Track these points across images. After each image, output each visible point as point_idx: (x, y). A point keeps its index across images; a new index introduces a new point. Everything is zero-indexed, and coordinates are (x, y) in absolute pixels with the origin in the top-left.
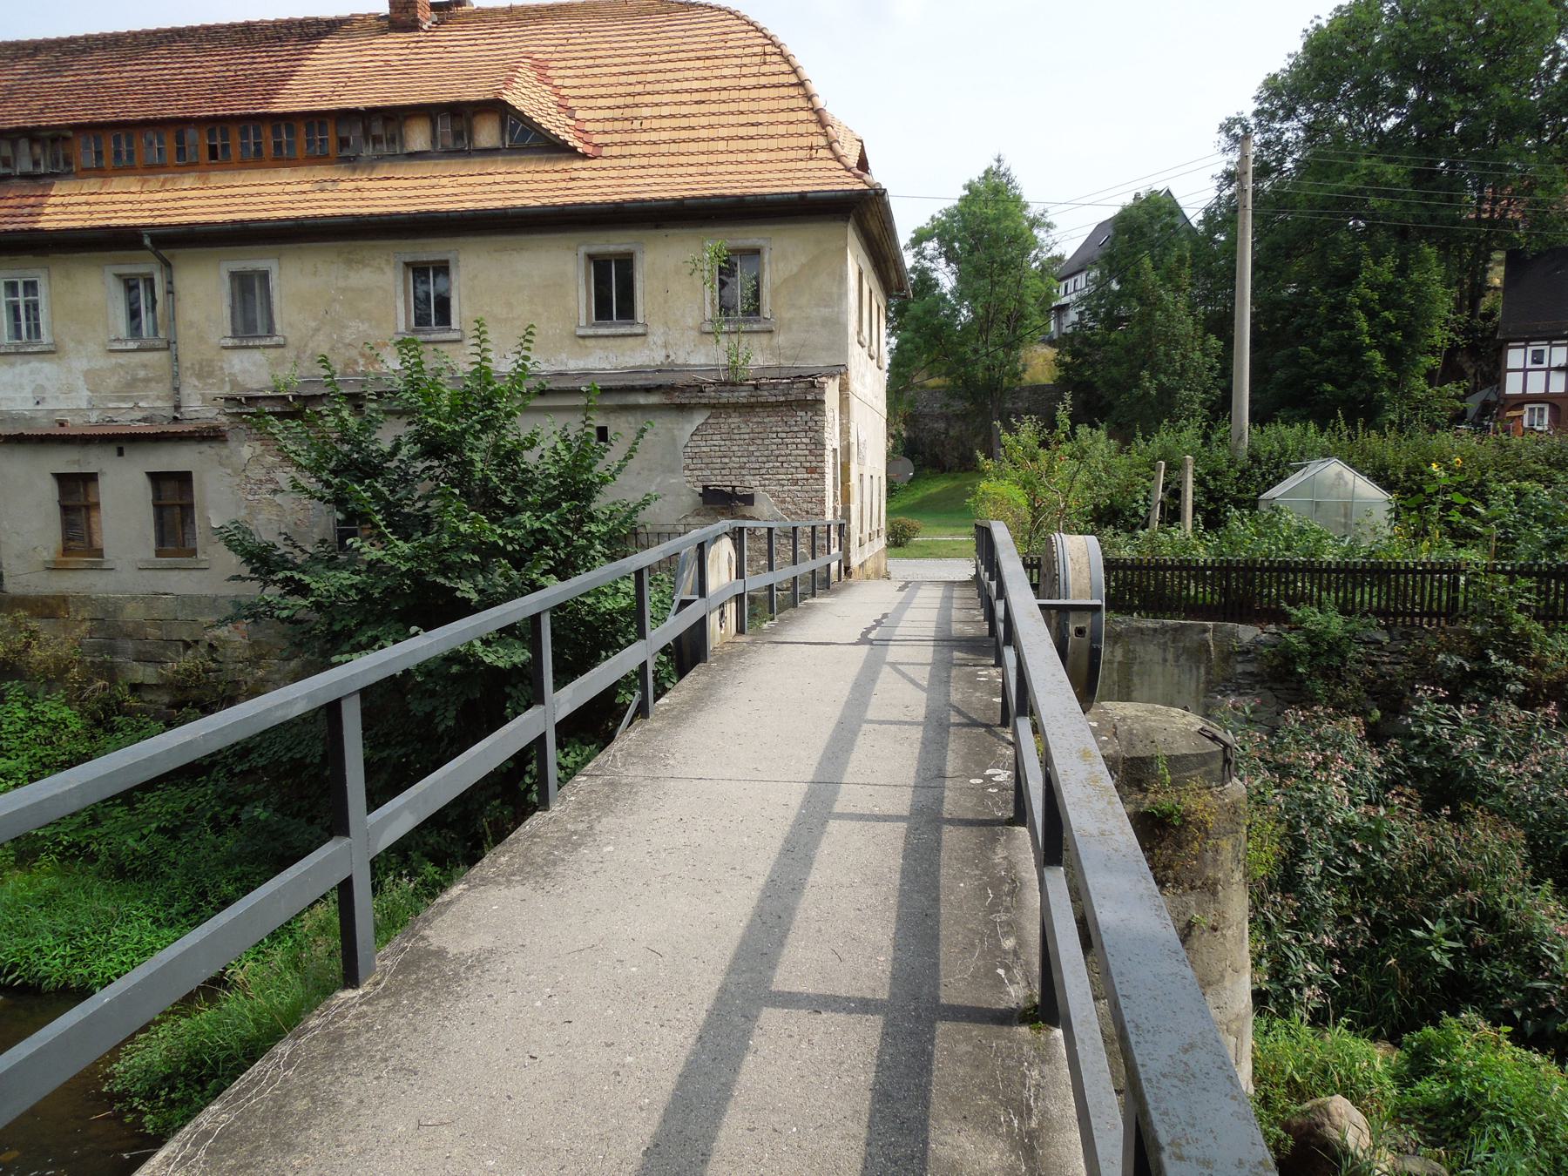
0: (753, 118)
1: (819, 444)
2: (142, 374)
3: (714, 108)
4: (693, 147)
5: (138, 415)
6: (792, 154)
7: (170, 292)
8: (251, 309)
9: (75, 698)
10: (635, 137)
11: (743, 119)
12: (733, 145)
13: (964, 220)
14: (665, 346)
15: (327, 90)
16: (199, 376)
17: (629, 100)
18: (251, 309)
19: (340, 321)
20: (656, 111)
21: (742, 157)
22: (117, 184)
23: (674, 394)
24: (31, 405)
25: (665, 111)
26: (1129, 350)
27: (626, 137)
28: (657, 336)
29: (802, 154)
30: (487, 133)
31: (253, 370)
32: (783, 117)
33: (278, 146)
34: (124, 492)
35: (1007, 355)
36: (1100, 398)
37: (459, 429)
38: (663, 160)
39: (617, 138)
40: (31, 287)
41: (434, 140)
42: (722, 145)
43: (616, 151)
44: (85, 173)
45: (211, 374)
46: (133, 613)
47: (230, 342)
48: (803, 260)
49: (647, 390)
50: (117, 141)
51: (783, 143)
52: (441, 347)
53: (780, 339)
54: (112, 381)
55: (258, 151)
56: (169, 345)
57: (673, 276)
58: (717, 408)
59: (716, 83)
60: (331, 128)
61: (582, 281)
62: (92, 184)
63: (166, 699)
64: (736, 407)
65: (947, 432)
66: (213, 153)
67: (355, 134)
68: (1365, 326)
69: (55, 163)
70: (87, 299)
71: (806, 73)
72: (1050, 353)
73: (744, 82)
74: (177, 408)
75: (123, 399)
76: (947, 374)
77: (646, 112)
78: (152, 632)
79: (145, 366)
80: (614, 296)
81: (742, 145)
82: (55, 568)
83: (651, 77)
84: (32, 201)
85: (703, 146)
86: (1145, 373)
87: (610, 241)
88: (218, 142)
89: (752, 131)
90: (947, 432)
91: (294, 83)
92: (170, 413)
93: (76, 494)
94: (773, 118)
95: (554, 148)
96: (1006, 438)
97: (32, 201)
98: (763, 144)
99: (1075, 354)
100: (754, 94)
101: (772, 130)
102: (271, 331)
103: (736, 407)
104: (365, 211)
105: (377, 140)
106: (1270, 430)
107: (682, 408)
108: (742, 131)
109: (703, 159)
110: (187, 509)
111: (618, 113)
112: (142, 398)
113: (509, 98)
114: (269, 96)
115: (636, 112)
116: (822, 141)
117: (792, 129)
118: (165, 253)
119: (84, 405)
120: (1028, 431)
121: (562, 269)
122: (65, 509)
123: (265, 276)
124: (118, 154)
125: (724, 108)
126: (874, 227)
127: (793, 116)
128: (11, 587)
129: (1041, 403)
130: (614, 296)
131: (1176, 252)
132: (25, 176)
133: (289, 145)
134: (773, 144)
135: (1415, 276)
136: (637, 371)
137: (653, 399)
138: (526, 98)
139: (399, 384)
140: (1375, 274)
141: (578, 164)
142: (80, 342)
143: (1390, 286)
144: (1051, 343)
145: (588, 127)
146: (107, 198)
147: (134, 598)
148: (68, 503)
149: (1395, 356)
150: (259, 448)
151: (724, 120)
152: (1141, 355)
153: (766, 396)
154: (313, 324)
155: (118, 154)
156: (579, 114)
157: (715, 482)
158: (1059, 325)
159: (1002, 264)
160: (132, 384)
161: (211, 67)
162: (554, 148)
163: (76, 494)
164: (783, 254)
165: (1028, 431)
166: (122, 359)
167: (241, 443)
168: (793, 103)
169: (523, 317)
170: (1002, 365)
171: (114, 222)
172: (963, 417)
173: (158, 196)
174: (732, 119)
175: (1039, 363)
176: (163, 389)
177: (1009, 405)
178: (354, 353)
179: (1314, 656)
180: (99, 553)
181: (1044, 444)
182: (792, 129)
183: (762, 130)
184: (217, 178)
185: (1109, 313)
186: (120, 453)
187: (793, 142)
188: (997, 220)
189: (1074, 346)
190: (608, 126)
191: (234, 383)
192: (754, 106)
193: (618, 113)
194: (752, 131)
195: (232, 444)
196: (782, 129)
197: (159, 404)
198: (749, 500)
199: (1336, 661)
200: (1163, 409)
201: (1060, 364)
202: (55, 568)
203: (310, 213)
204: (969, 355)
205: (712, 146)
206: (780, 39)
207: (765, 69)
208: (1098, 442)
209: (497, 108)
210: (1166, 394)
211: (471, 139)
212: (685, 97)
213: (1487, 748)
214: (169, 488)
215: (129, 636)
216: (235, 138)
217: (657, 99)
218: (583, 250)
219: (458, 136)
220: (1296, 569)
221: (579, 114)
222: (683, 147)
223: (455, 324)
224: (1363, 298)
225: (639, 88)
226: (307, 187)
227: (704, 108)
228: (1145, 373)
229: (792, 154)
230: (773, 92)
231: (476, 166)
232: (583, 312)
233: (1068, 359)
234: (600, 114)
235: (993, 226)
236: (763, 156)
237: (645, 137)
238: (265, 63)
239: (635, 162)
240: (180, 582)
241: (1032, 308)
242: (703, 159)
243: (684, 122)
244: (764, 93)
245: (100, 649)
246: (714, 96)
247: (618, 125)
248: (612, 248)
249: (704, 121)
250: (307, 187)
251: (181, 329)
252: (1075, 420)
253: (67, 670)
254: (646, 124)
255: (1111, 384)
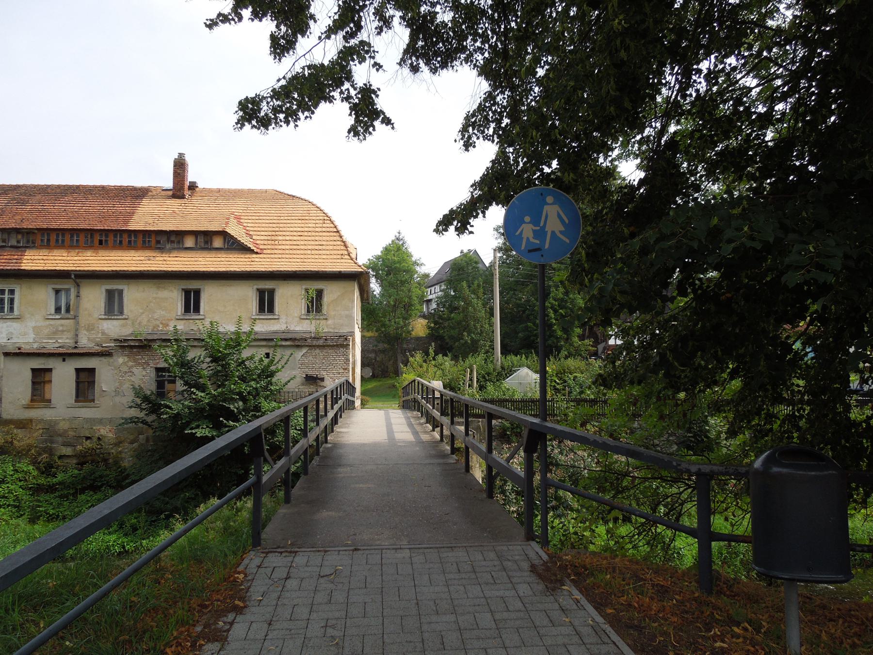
0: (320, 243)
1: (348, 360)
2: (61, 328)
3: (306, 238)
4: (298, 252)
5: (57, 345)
6: (335, 257)
7: (78, 296)
8: (114, 305)
9: (34, 462)
10: (276, 247)
11: (317, 243)
12: (313, 252)
13: (383, 261)
14: (286, 323)
15: (151, 221)
16: (88, 330)
17: (274, 233)
18: (114, 305)
19: (154, 311)
20: (284, 238)
21: (317, 257)
22: (56, 252)
23: (296, 342)
24: (5, 340)
25: (288, 238)
26: (459, 323)
27: (273, 247)
28: (283, 319)
29: (339, 257)
30: (218, 242)
31: (114, 328)
32: (331, 243)
33: (130, 242)
34: (63, 377)
35: (404, 322)
36: (447, 343)
37: (222, 352)
38: (287, 256)
39: (269, 247)
40: (12, 292)
41: (196, 243)
42: (309, 252)
43: (269, 251)
44: (41, 247)
45: (93, 329)
46: (63, 426)
47: (103, 317)
48: (339, 294)
49: (286, 340)
50: (58, 235)
51: (332, 252)
52: (197, 321)
53: (330, 322)
54: (46, 331)
55: (121, 242)
56: (75, 317)
57: (291, 300)
58: (311, 347)
59: (306, 229)
60: (153, 236)
61: (254, 298)
62: (44, 252)
63: (75, 461)
64: (319, 347)
65: (375, 359)
66: (101, 242)
67: (163, 239)
68: (553, 316)
69: (28, 242)
70: (42, 296)
71: (339, 228)
72: (424, 322)
73: (317, 229)
74: (76, 343)
75: (51, 339)
76: (377, 331)
77: (280, 238)
78: (71, 433)
79: (62, 325)
80: (266, 303)
81: (317, 252)
82: (27, 407)
83: (281, 225)
84: (16, 257)
85: (302, 252)
86: (465, 333)
87: (266, 286)
88: (104, 239)
89: (320, 247)
90: (375, 359)
91: (135, 217)
92: (73, 345)
93: (40, 378)
94: (328, 243)
95: (245, 249)
96: (411, 359)
97: (16, 257)
98: (324, 252)
99: (436, 323)
100: (321, 234)
101: (328, 247)
102: (121, 312)
103: (319, 347)
104: (170, 269)
105: (173, 242)
106: (508, 358)
107: (298, 346)
108: (317, 247)
109: (302, 256)
110: (92, 383)
111: (269, 238)
112: (60, 338)
113: (228, 230)
114: (126, 222)
115: (276, 238)
116: (346, 253)
117: (335, 247)
118: (78, 281)
119: (31, 341)
120: (419, 357)
121: (248, 294)
122: (33, 383)
123: (121, 292)
124: (57, 241)
125: (309, 238)
126: (362, 281)
127: (335, 243)
128: (5, 416)
129: (422, 345)
130: (266, 303)
131: (476, 282)
132: (12, 247)
133: (135, 242)
134: (328, 252)
135: (571, 296)
136: (276, 332)
137: (288, 343)
138: (234, 230)
139: (204, 336)
140: (556, 295)
141: (254, 256)
142: (33, 315)
143: (562, 300)
144: (424, 317)
145: (258, 242)
146: (52, 258)
147: (64, 420)
148: (38, 380)
149: (565, 330)
150: (126, 359)
151: (310, 243)
152: (464, 326)
153: (329, 343)
154: (141, 311)
155: (57, 241)
156: (254, 237)
157: (310, 373)
158: (428, 308)
159: (401, 281)
160: (55, 333)
161: (95, 206)
162: (245, 249)
163: (40, 378)
164: (331, 292)
165: (419, 357)
166: (52, 322)
167: (119, 357)
168: (335, 238)
169: (227, 312)
170: (402, 328)
171: (57, 268)
172: (383, 351)
173: (76, 258)
174: (313, 243)
175: (419, 327)
176: (71, 335)
177: (405, 346)
178: (158, 322)
179: (513, 429)
180: (49, 401)
181: (425, 361)
182: (335, 247)
183: (324, 247)
184: (102, 253)
185: (450, 306)
186: (64, 360)
187: (336, 252)
188: (399, 262)
189: (434, 318)
190: (266, 242)
191: (103, 333)
192: (321, 238)
193: (269, 238)
194: (320, 247)
195: (115, 358)
196: (331, 247)
197: (67, 341)
198: (322, 379)
199: (519, 430)
200: (473, 348)
201: (429, 327)
202: (27, 407)
203: (146, 269)
204: (387, 322)
205: (306, 252)
206: (329, 215)
207: (324, 225)
208: (447, 362)
209: (224, 234)
210: (475, 342)
211: (211, 244)
212: (295, 234)
213: (561, 453)
214: (83, 376)
215: (60, 435)
216: (111, 238)
217: (284, 233)
218: (255, 287)
219: (206, 242)
220: (507, 401)
221: (254, 237)
222: (295, 252)
223: (202, 312)
224: (552, 304)
225: (277, 229)
226: (142, 258)
227: (302, 238)
228: (465, 333)
229: (335, 257)
230: (328, 234)
231: (213, 254)
232: (254, 310)
233: (432, 325)
234: (263, 238)
235: (398, 265)
236: (324, 257)
237: (280, 247)
238: (121, 207)
239: (276, 256)
240: (86, 413)
241: (415, 301)
242: (302, 256)
243: (295, 243)
244: (324, 234)
245: (46, 441)
246: (306, 234)
247: (270, 242)
248: (267, 287)
249: (302, 243)
250: (142, 258)
251: (81, 311)
252: (436, 354)
253: (30, 450)
254: (280, 242)
255: (450, 337)
